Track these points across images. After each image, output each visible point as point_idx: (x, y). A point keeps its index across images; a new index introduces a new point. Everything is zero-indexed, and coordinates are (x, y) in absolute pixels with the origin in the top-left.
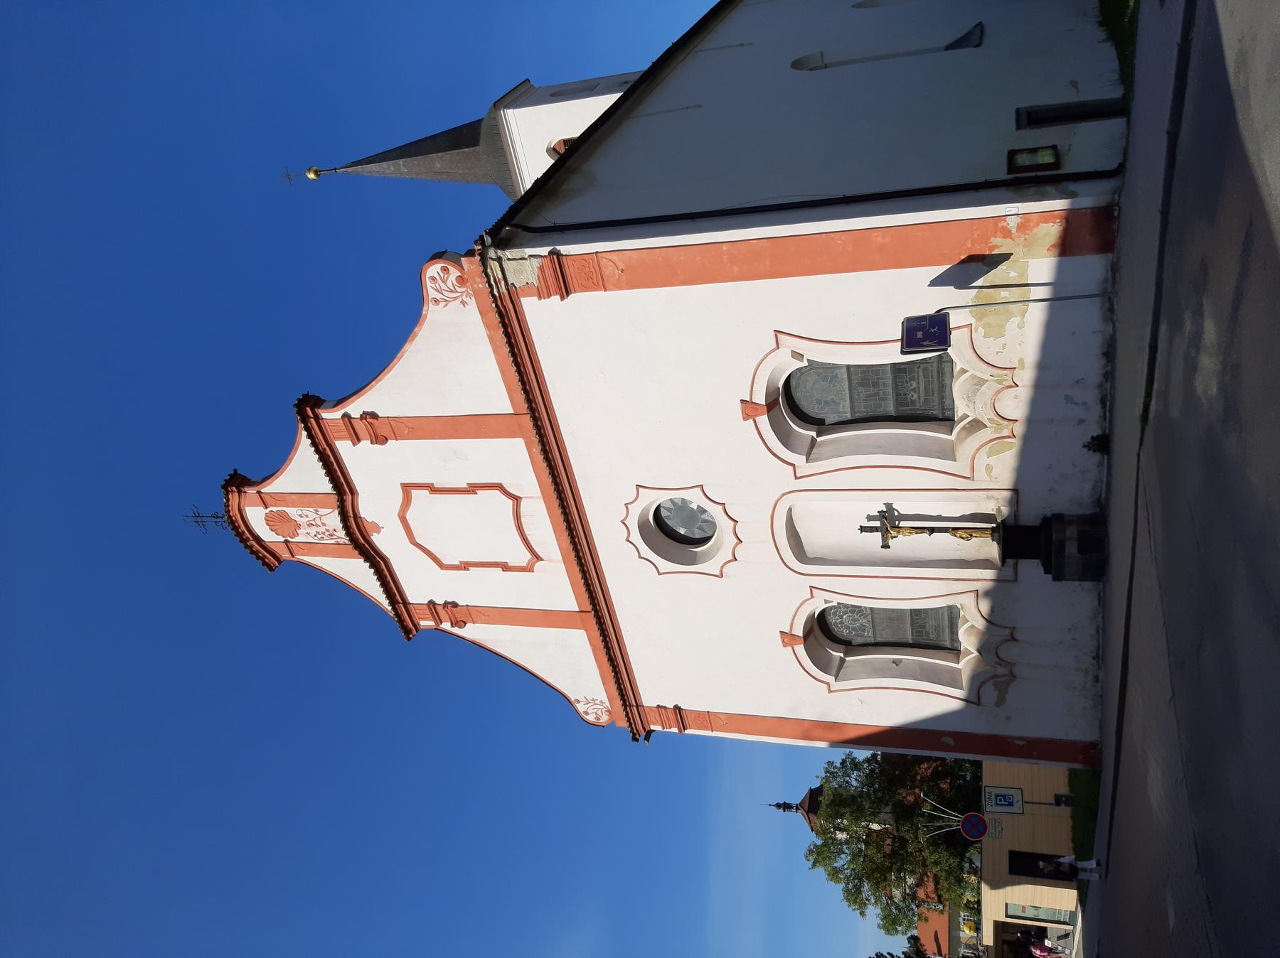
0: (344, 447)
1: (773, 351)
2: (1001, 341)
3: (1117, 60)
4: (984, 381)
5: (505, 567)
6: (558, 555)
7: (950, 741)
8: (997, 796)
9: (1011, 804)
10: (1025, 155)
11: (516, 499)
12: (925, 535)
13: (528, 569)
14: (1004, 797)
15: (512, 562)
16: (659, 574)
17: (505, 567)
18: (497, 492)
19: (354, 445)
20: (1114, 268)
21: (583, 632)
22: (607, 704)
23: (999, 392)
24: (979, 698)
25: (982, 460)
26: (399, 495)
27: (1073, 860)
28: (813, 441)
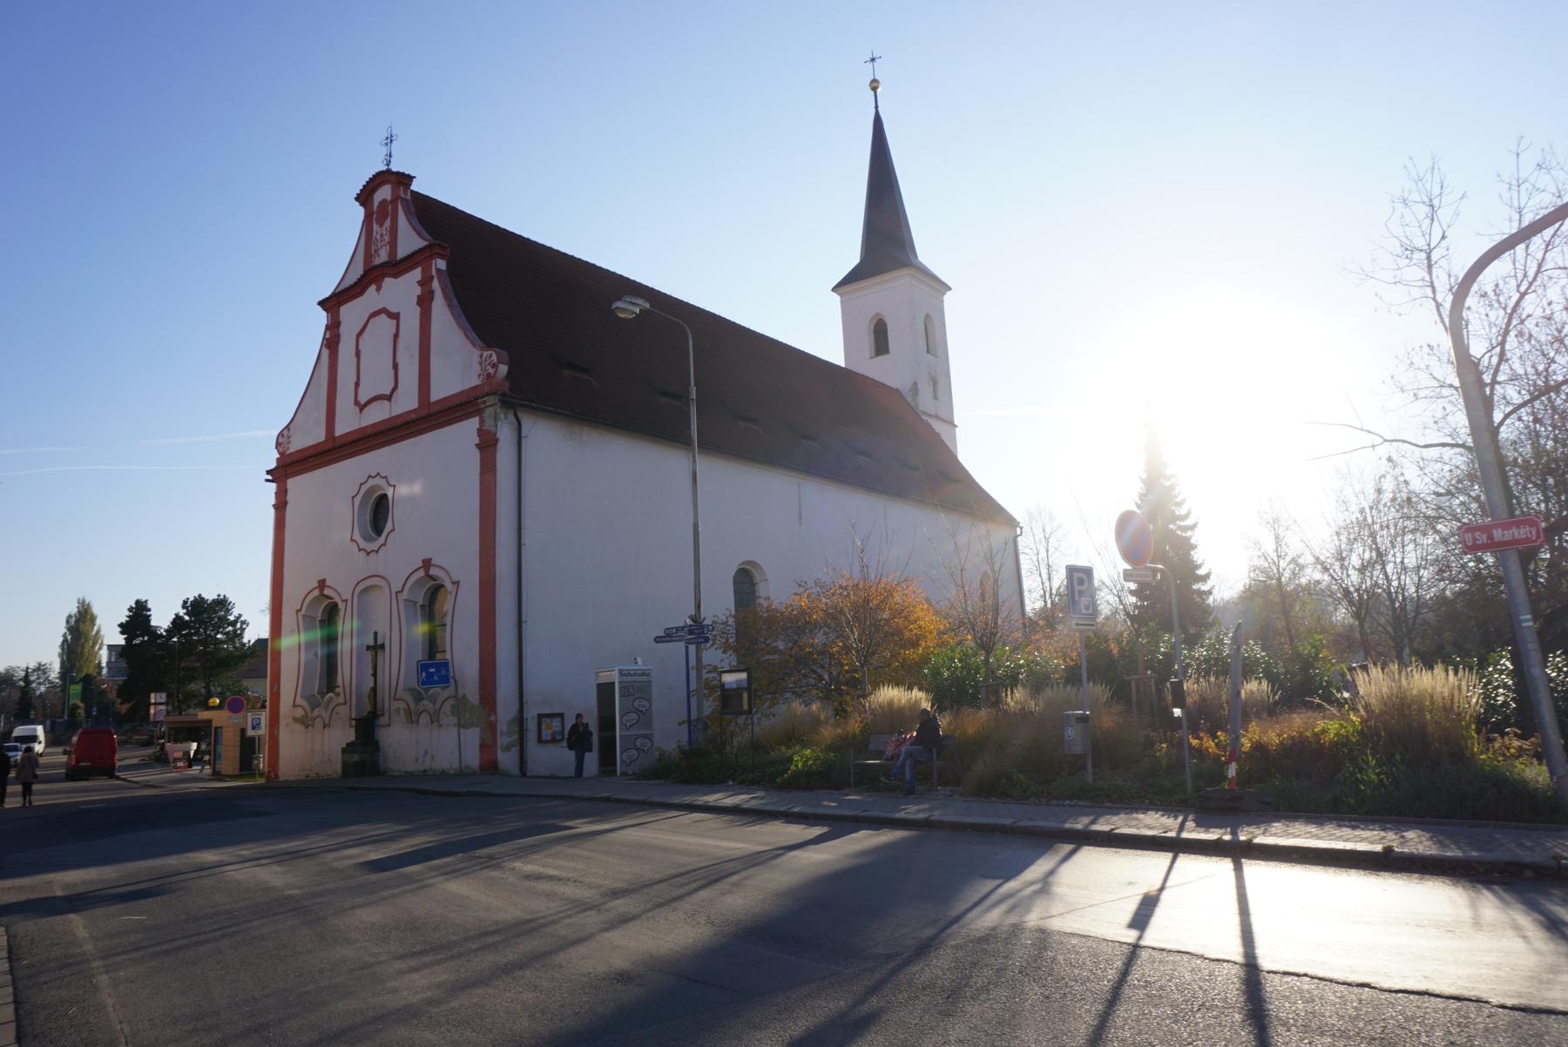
0: (416, 274)
1: (451, 579)
2: (449, 714)
3: (238, 748)
4: (434, 704)
5: (357, 385)
6: (364, 424)
7: (275, 689)
8: (259, 719)
9: (254, 728)
10: (559, 724)
11: (389, 398)
12: (371, 672)
13: (356, 402)
14: (259, 724)
15: (361, 389)
16: (353, 497)
17: (357, 385)
18: (393, 385)
19: (418, 282)
20: (474, 774)
21: (416, 405)
22: (288, 452)
23: (429, 714)
24: (398, 700)
25: (402, 705)
26: (394, 310)
27: (118, 752)
28: (315, 618)
